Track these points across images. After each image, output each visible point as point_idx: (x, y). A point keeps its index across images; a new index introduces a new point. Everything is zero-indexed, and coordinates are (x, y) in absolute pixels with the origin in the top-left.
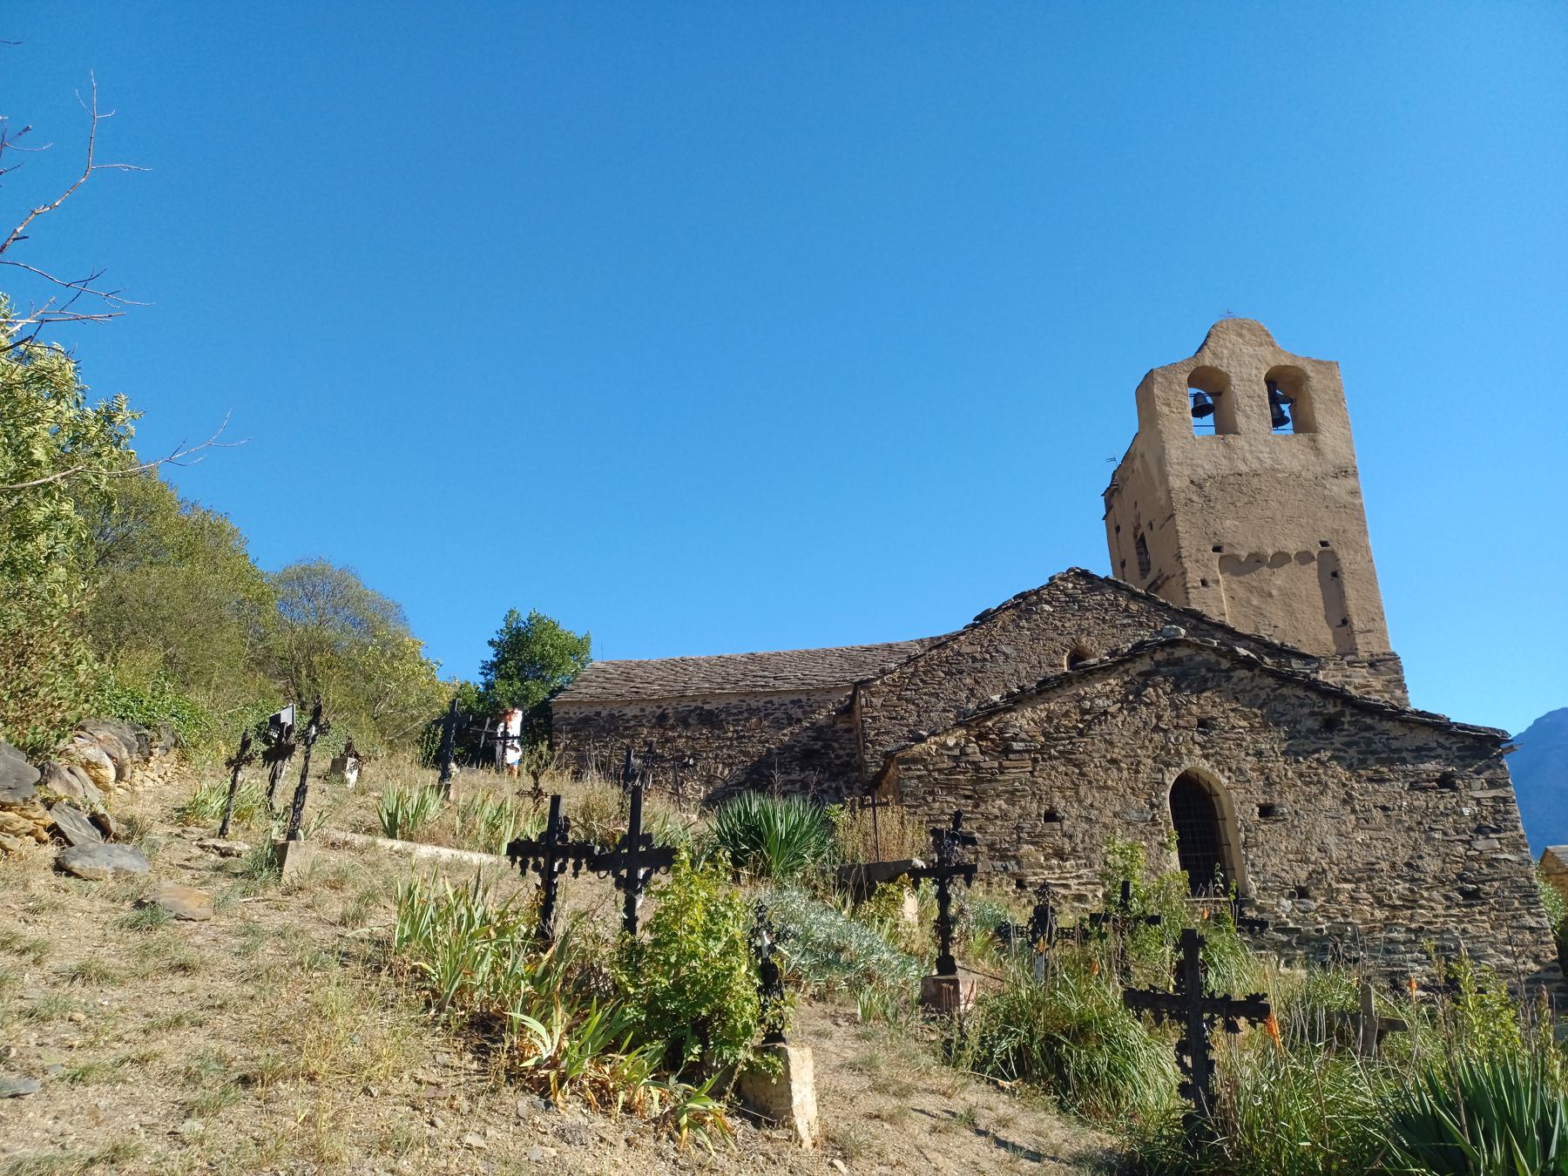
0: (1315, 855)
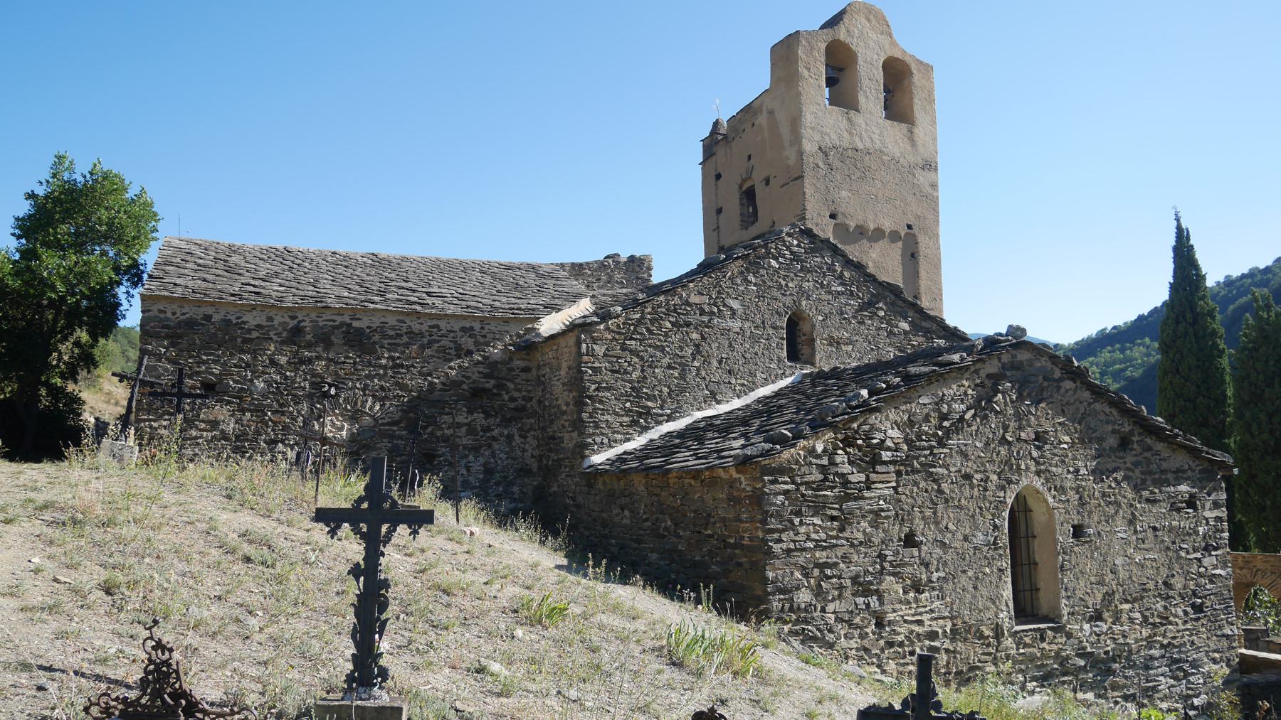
0: (1109, 577)
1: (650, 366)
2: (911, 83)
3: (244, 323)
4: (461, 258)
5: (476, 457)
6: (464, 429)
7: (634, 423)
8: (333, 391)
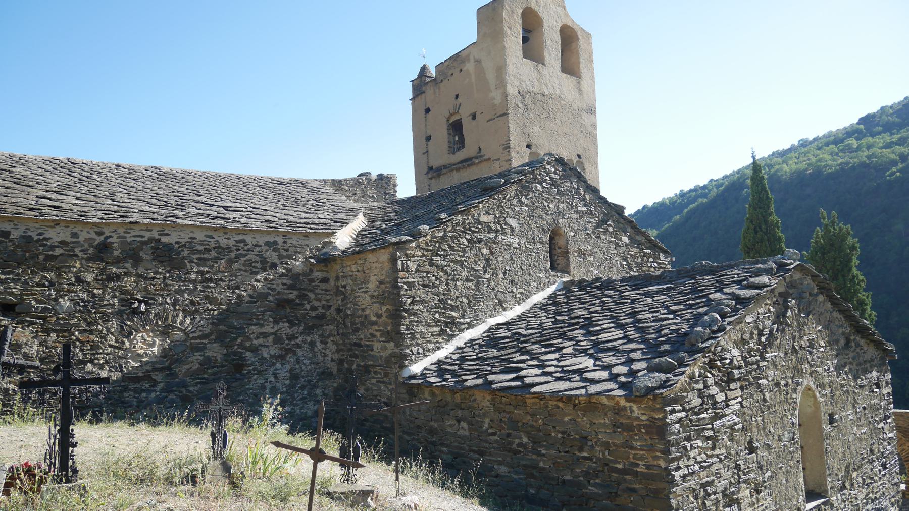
1: (453, 280)
2: (577, 46)
3: (47, 239)
4: (237, 173)
5: (282, 364)
6: (271, 339)
7: (442, 332)
8: (143, 307)
